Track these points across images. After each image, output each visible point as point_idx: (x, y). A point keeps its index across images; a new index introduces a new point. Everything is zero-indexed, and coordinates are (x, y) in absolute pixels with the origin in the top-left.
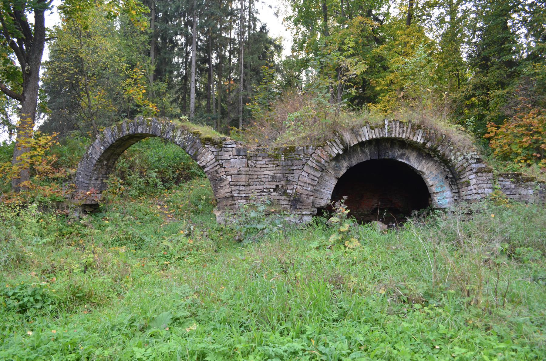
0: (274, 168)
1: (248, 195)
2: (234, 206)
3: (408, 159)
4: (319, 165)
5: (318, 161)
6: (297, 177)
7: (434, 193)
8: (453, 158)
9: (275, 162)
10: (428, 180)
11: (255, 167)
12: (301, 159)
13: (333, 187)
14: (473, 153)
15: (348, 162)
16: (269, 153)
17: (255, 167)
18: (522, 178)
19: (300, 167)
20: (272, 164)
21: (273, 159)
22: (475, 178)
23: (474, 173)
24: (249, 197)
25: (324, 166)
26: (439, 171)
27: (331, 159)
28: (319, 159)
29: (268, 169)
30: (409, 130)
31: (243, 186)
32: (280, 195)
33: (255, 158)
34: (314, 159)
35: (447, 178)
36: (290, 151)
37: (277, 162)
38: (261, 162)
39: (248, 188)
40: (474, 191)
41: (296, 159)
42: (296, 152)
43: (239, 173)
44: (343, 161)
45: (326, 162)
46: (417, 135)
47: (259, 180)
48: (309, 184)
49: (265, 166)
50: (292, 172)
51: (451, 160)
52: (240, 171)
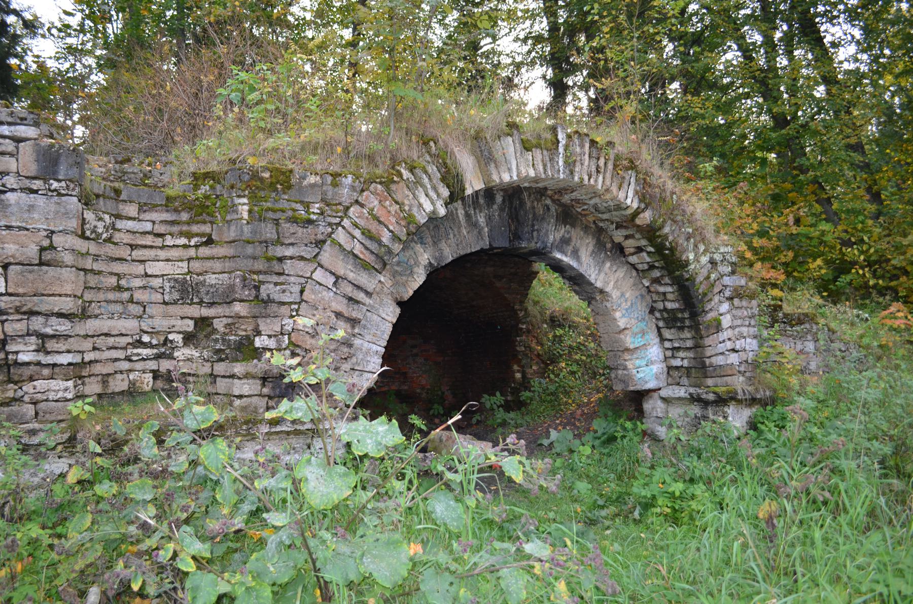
0: (192, 252)
1: (77, 359)
2: (15, 408)
3: (575, 254)
4: (373, 246)
5: (368, 234)
6: (297, 289)
7: (627, 350)
8: (691, 257)
9: (195, 228)
10: (618, 315)
11: (109, 240)
12: (310, 222)
13: (388, 329)
14: (726, 250)
15: (430, 249)
16: (171, 192)
17: (109, 240)
18: (786, 315)
19: (308, 252)
20: (181, 234)
21: (185, 216)
22: (728, 312)
23: (727, 299)
24: (83, 364)
25: (390, 252)
26: (638, 293)
27: (412, 228)
28: (373, 227)
29: (162, 254)
30: (610, 166)
31: (60, 315)
32: (220, 356)
33: (110, 205)
34: (356, 225)
35: (652, 311)
36: (272, 186)
37: (207, 229)
38: (135, 223)
39: (83, 327)
40: (729, 345)
41: (294, 220)
42: (292, 192)
43: (47, 256)
44: (419, 248)
45: (395, 238)
46: (625, 186)
47: (126, 299)
48: (338, 315)
49: (149, 240)
50: (277, 268)
51: (687, 263)
52: (52, 247)
